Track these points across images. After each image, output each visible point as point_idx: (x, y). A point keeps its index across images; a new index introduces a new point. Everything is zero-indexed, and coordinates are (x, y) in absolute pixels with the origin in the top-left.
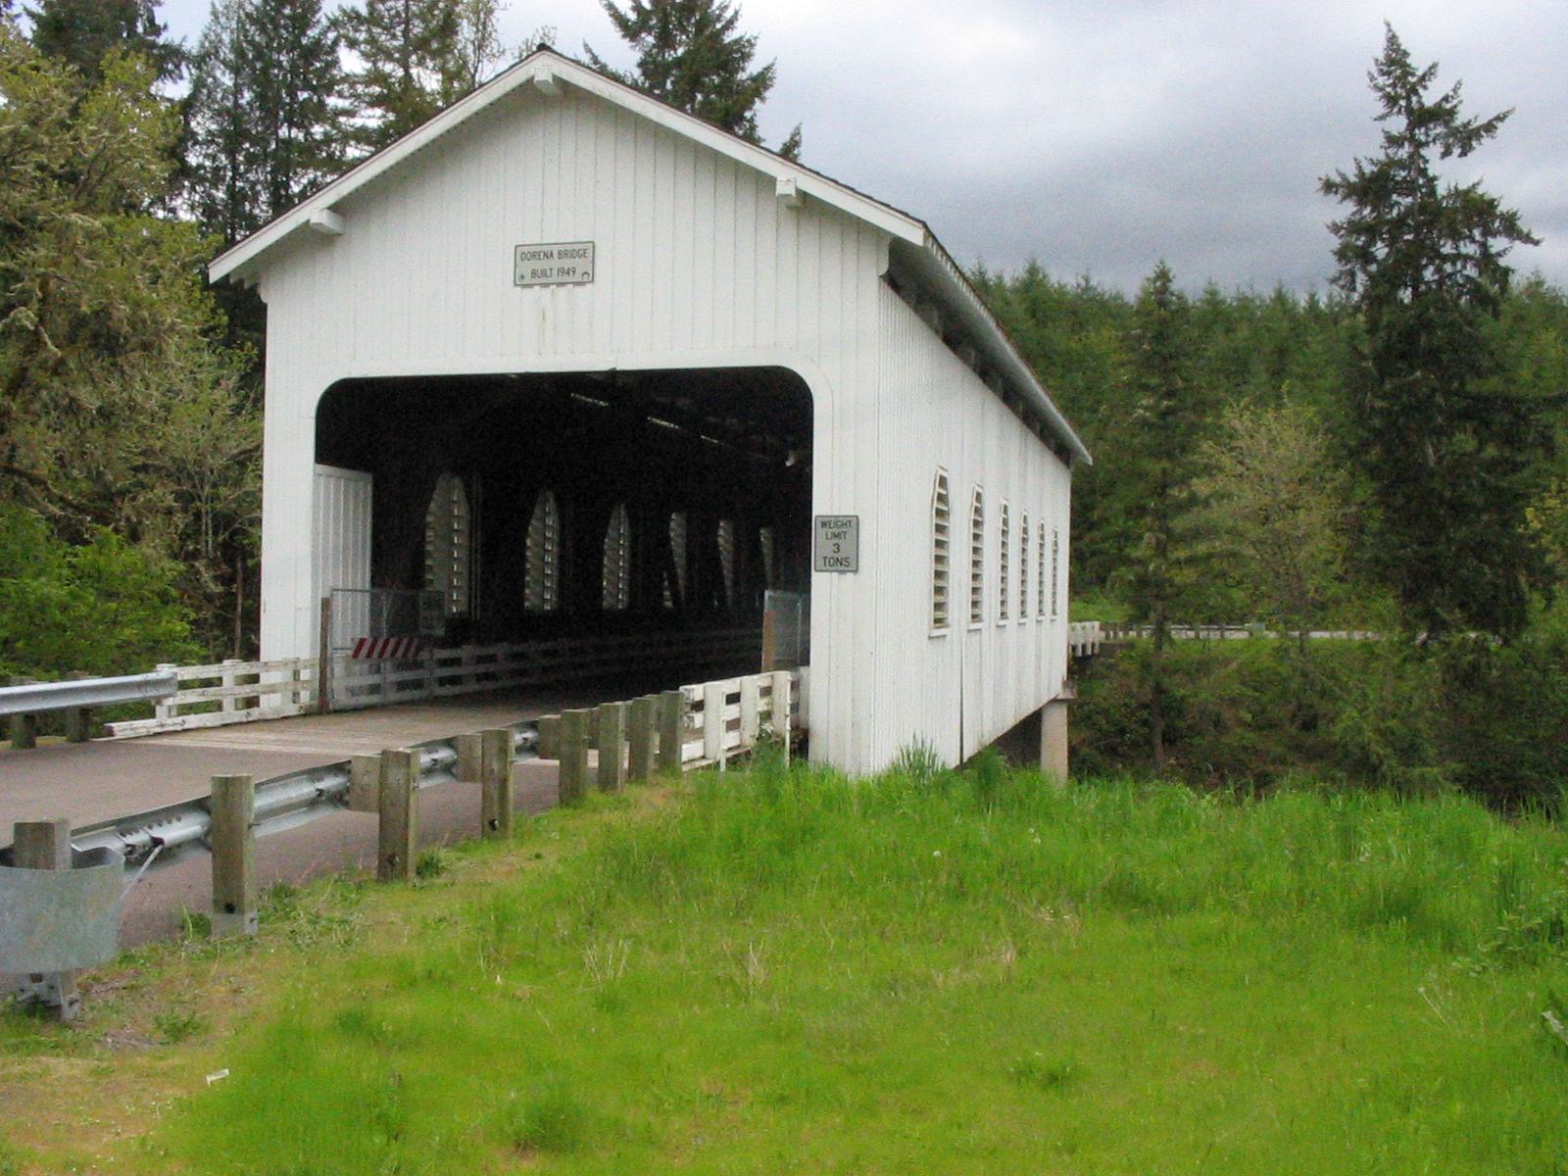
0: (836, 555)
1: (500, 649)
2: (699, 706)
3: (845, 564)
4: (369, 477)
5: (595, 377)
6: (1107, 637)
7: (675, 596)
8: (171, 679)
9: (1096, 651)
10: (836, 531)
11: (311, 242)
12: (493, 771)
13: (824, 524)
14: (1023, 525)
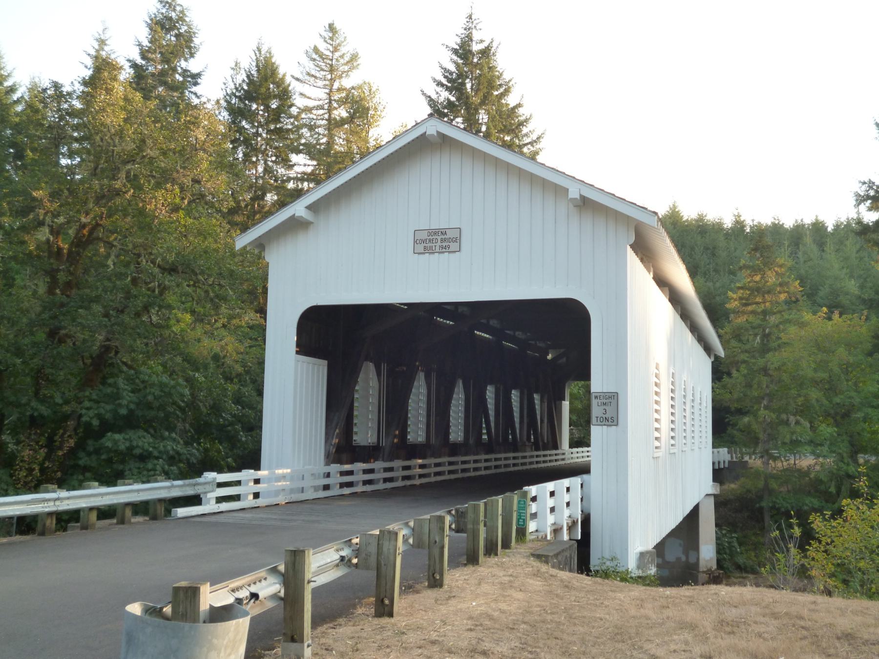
0: (604, 416)
1: (397, 463)
2: (534, 499)
3: (612, 420)
4: (494, 386)
5: (448, 307)
6: (732, 457)
7: (489, 433)
8: (213, 481)
9: (727, 465)
10: (605, 401)
11: (295, 225)
12: (436, 542)
13: (596, 397)
14: (692, 398)
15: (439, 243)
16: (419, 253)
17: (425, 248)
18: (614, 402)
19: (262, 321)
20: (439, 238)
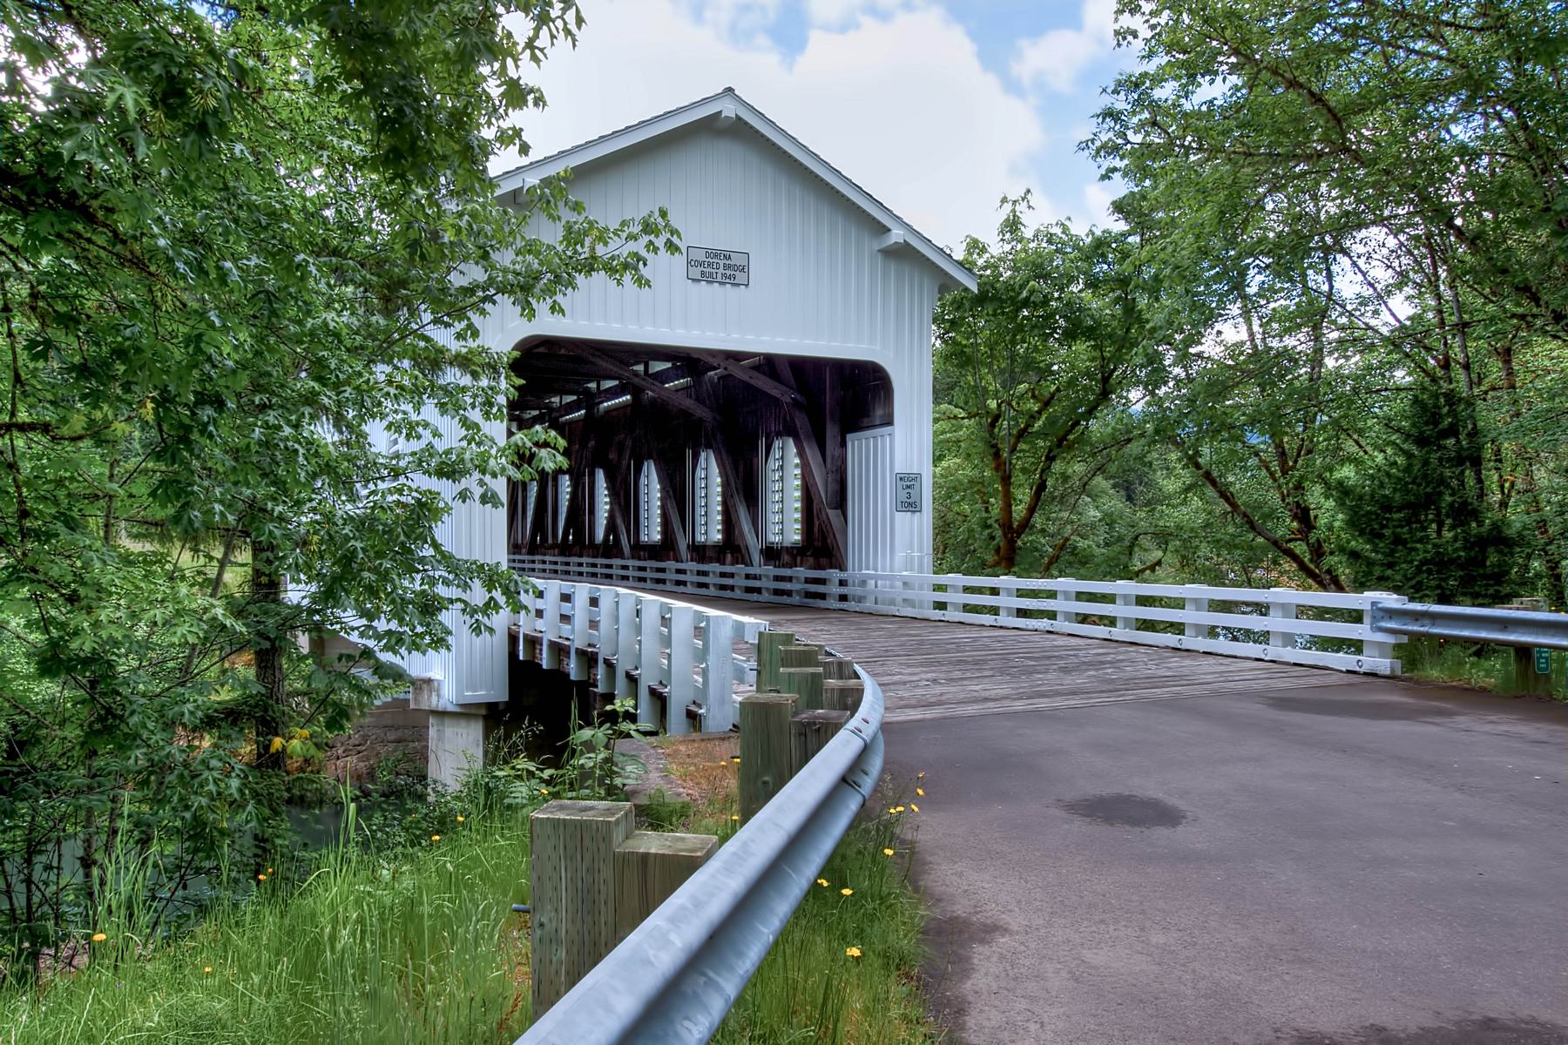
15: (721, 270)
16: (693, 280)
17: (703, 273)
18: (917, 485)
19: (563, 989)
20: (721, 263)
